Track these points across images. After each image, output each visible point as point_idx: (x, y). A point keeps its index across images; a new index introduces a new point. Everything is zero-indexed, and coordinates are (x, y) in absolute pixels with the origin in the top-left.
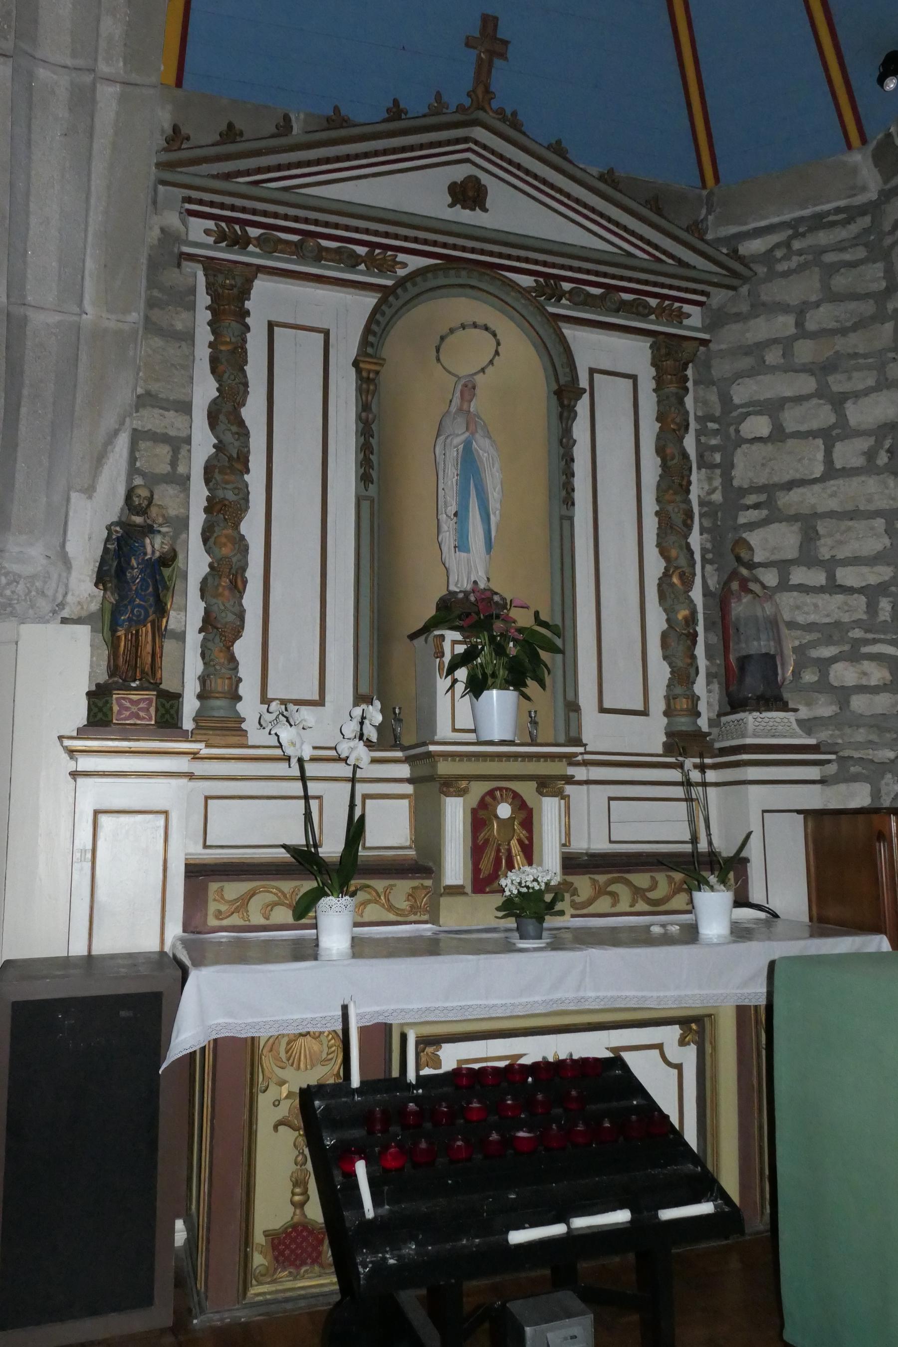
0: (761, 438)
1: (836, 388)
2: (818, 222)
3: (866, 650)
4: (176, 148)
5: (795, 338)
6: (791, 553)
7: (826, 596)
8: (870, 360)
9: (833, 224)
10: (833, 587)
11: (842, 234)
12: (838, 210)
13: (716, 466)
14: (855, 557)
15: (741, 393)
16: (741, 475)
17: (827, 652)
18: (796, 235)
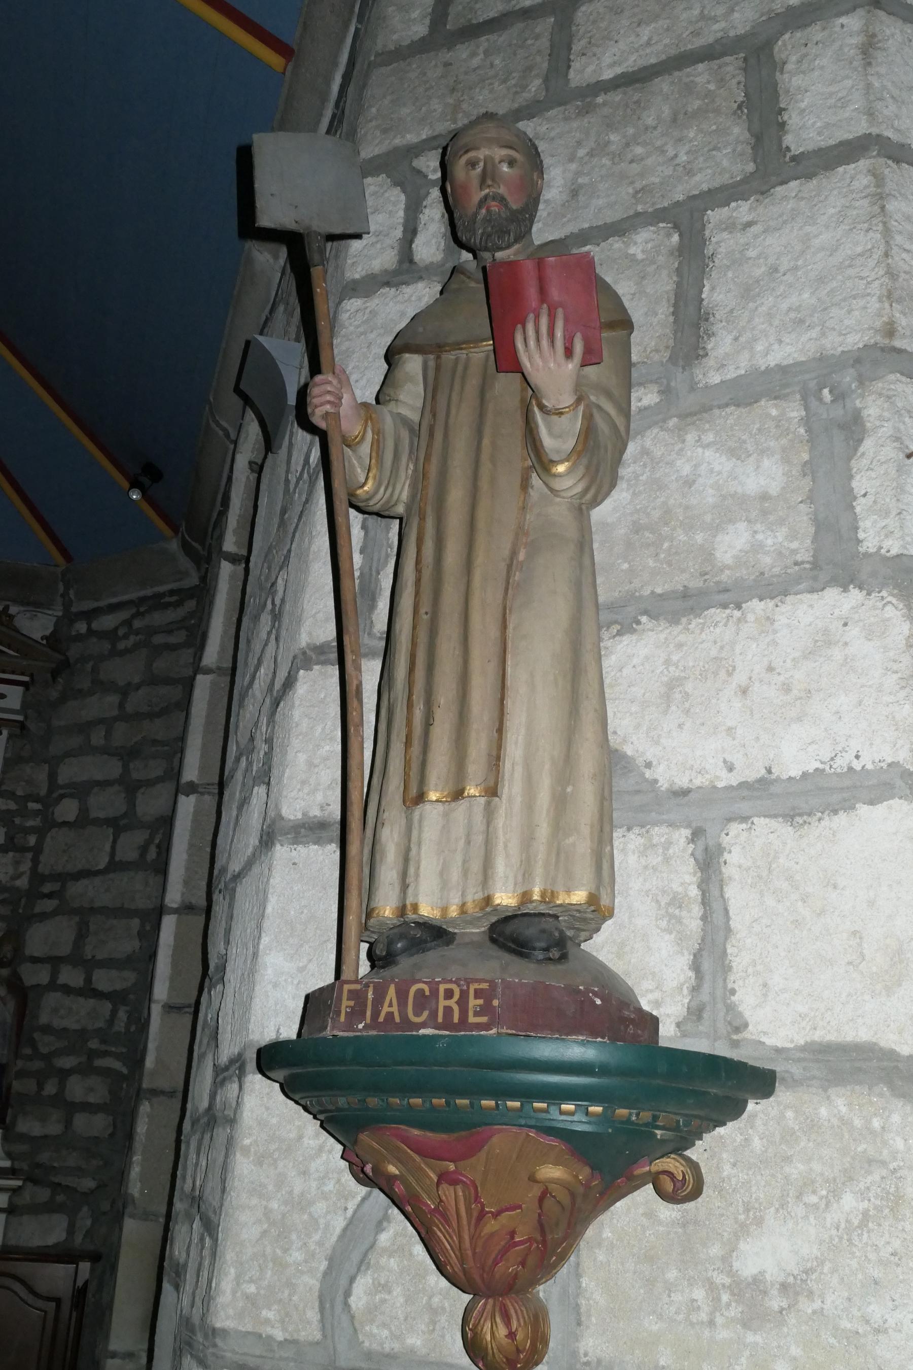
0: (68, 822)
1: (135, 775)
2: (157, 603)
3: (99, 1062)
4: (232, 446)
5: (115, 719)
6: (65, 950)
7: (81, 1000)
8: (166, 748)
9: (167, 605)
10: (89, 991)
11: (171, 615)
12: (172, 592)
13: (29, 849)
14: (111, 959)
15: (68, 773)
16: (49, 862)
17: (67, 1062)
18: (138, 614)
